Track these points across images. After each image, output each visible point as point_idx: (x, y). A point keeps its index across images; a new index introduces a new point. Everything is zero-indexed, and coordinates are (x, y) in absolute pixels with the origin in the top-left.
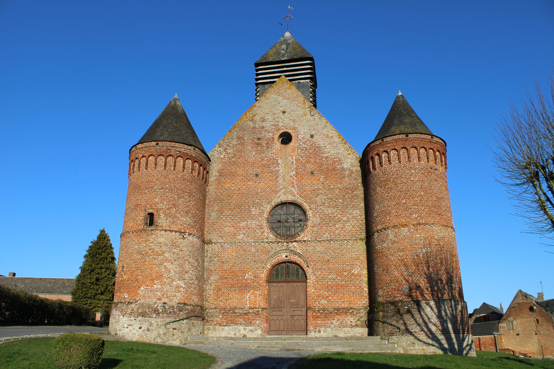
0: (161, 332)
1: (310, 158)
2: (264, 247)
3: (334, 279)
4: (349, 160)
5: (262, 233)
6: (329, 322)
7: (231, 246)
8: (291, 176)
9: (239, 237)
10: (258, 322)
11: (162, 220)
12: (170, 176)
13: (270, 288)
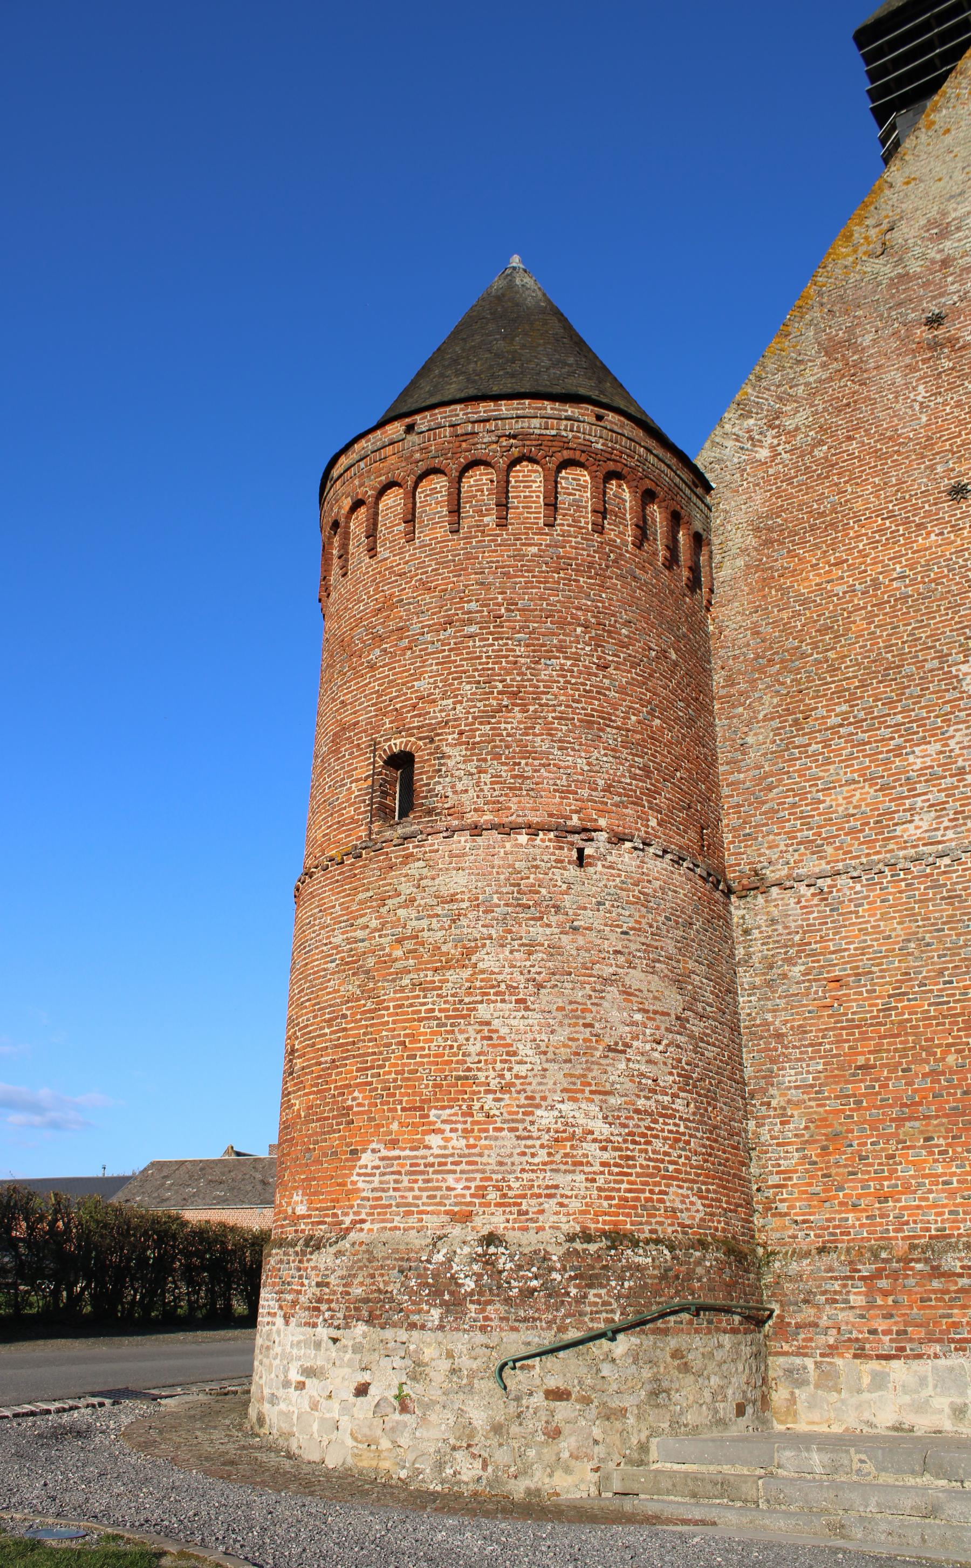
0: (479, 1417)
7: (871, 885)
9: (910, 831)
11: (455, 780)
12: (484, 558)
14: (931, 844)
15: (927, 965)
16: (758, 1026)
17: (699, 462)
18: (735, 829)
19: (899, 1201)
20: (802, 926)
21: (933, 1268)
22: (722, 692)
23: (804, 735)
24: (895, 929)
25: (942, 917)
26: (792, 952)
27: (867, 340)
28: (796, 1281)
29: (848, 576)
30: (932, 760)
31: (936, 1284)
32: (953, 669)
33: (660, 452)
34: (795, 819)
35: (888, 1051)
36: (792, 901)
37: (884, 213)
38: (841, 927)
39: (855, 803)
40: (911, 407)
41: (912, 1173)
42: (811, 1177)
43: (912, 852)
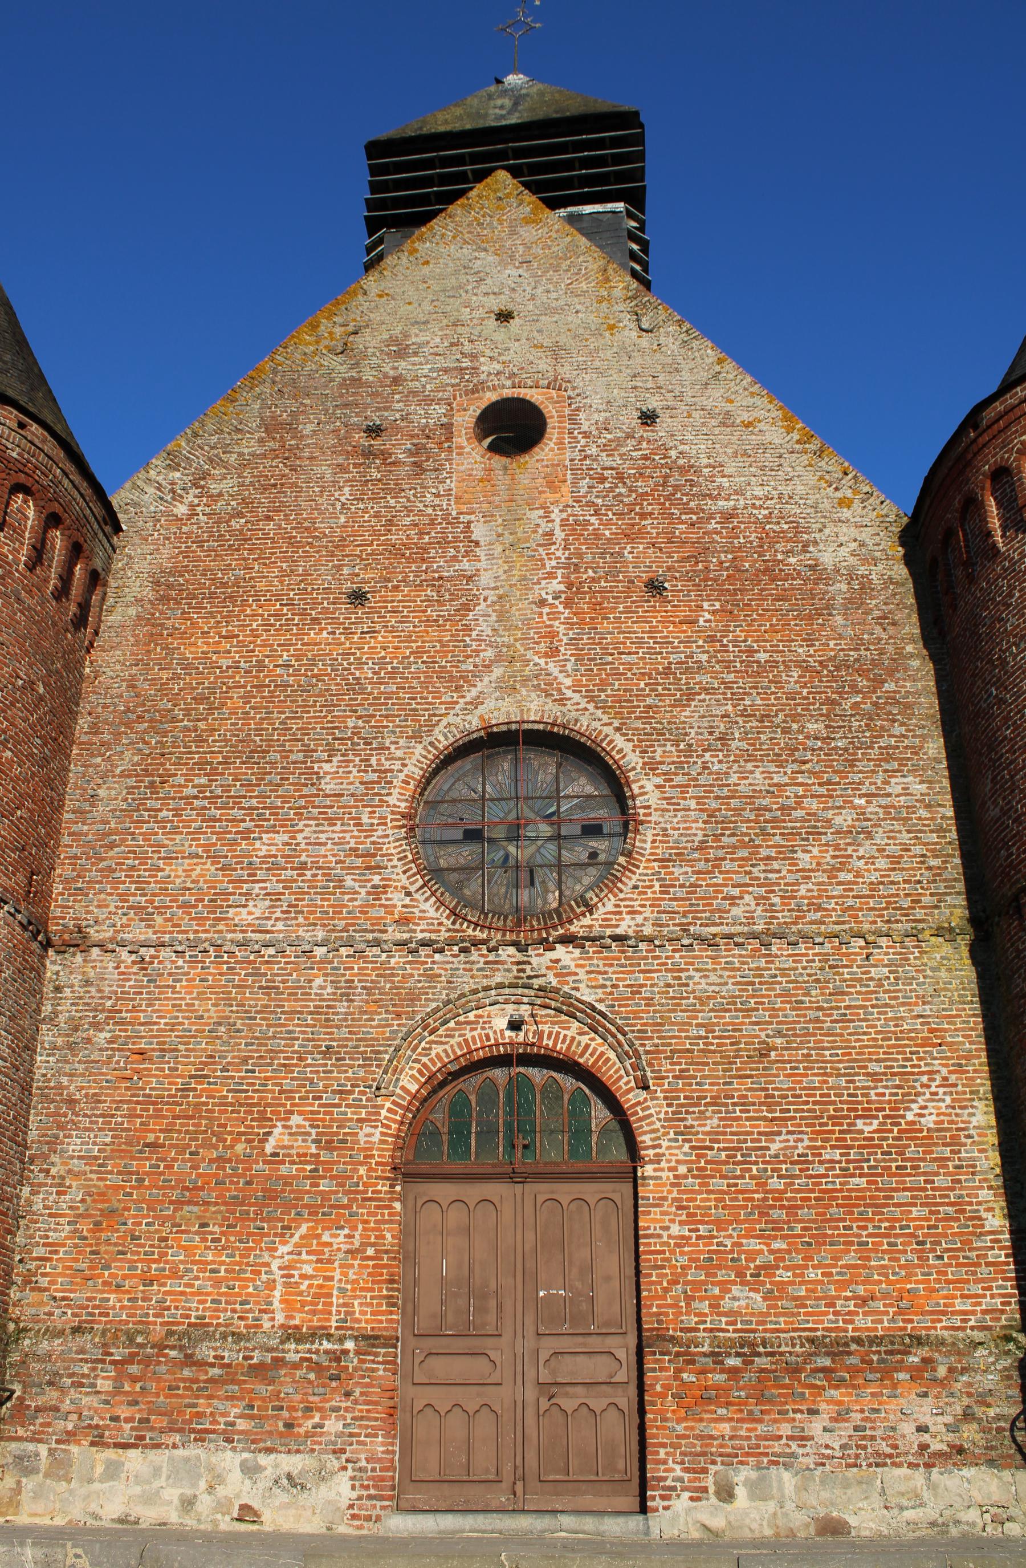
1: (643, 516)
2: (385, 972)
3: (802, 1160)
4: (846, 532)
5: (378, 891)
6: (785, 1429)
7: (193, 962)
8: (542, 603)
10: (333, 1426)
13: (413, 1212)
14: (260, 932)
15: (233, 1051)
16: (52, 1088)
17: (115, 501)
18: (67, 881)
19: (164, 1285)
20: (116, 992)
21: (186, 1356)
22: (85, 738)
23: (157, 799)
24: (208, 1011)
25: (256, 1006)
26: (101, 1017)
27: (308, 429)
28: (44, 1361)
29: (236, 652)
30: (278, 850)
31: (187, 1373)
32: (316, 766)
33: (77, 478)
34: (131, 883)
35: (179, 1132)
36: (111, 965)
37: (352, 316)
38: (156, 999)
39: (194, 877)
40: (333, 505)
41: (182, 1258)
42: (79, 1253)
43: (240, 936)
